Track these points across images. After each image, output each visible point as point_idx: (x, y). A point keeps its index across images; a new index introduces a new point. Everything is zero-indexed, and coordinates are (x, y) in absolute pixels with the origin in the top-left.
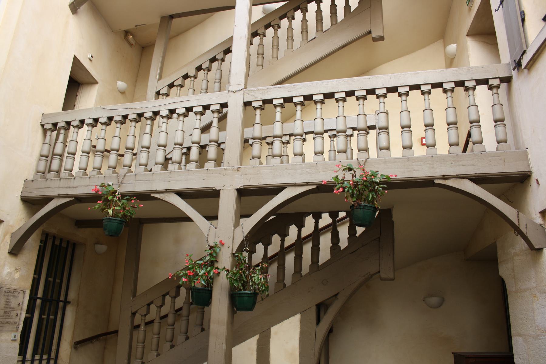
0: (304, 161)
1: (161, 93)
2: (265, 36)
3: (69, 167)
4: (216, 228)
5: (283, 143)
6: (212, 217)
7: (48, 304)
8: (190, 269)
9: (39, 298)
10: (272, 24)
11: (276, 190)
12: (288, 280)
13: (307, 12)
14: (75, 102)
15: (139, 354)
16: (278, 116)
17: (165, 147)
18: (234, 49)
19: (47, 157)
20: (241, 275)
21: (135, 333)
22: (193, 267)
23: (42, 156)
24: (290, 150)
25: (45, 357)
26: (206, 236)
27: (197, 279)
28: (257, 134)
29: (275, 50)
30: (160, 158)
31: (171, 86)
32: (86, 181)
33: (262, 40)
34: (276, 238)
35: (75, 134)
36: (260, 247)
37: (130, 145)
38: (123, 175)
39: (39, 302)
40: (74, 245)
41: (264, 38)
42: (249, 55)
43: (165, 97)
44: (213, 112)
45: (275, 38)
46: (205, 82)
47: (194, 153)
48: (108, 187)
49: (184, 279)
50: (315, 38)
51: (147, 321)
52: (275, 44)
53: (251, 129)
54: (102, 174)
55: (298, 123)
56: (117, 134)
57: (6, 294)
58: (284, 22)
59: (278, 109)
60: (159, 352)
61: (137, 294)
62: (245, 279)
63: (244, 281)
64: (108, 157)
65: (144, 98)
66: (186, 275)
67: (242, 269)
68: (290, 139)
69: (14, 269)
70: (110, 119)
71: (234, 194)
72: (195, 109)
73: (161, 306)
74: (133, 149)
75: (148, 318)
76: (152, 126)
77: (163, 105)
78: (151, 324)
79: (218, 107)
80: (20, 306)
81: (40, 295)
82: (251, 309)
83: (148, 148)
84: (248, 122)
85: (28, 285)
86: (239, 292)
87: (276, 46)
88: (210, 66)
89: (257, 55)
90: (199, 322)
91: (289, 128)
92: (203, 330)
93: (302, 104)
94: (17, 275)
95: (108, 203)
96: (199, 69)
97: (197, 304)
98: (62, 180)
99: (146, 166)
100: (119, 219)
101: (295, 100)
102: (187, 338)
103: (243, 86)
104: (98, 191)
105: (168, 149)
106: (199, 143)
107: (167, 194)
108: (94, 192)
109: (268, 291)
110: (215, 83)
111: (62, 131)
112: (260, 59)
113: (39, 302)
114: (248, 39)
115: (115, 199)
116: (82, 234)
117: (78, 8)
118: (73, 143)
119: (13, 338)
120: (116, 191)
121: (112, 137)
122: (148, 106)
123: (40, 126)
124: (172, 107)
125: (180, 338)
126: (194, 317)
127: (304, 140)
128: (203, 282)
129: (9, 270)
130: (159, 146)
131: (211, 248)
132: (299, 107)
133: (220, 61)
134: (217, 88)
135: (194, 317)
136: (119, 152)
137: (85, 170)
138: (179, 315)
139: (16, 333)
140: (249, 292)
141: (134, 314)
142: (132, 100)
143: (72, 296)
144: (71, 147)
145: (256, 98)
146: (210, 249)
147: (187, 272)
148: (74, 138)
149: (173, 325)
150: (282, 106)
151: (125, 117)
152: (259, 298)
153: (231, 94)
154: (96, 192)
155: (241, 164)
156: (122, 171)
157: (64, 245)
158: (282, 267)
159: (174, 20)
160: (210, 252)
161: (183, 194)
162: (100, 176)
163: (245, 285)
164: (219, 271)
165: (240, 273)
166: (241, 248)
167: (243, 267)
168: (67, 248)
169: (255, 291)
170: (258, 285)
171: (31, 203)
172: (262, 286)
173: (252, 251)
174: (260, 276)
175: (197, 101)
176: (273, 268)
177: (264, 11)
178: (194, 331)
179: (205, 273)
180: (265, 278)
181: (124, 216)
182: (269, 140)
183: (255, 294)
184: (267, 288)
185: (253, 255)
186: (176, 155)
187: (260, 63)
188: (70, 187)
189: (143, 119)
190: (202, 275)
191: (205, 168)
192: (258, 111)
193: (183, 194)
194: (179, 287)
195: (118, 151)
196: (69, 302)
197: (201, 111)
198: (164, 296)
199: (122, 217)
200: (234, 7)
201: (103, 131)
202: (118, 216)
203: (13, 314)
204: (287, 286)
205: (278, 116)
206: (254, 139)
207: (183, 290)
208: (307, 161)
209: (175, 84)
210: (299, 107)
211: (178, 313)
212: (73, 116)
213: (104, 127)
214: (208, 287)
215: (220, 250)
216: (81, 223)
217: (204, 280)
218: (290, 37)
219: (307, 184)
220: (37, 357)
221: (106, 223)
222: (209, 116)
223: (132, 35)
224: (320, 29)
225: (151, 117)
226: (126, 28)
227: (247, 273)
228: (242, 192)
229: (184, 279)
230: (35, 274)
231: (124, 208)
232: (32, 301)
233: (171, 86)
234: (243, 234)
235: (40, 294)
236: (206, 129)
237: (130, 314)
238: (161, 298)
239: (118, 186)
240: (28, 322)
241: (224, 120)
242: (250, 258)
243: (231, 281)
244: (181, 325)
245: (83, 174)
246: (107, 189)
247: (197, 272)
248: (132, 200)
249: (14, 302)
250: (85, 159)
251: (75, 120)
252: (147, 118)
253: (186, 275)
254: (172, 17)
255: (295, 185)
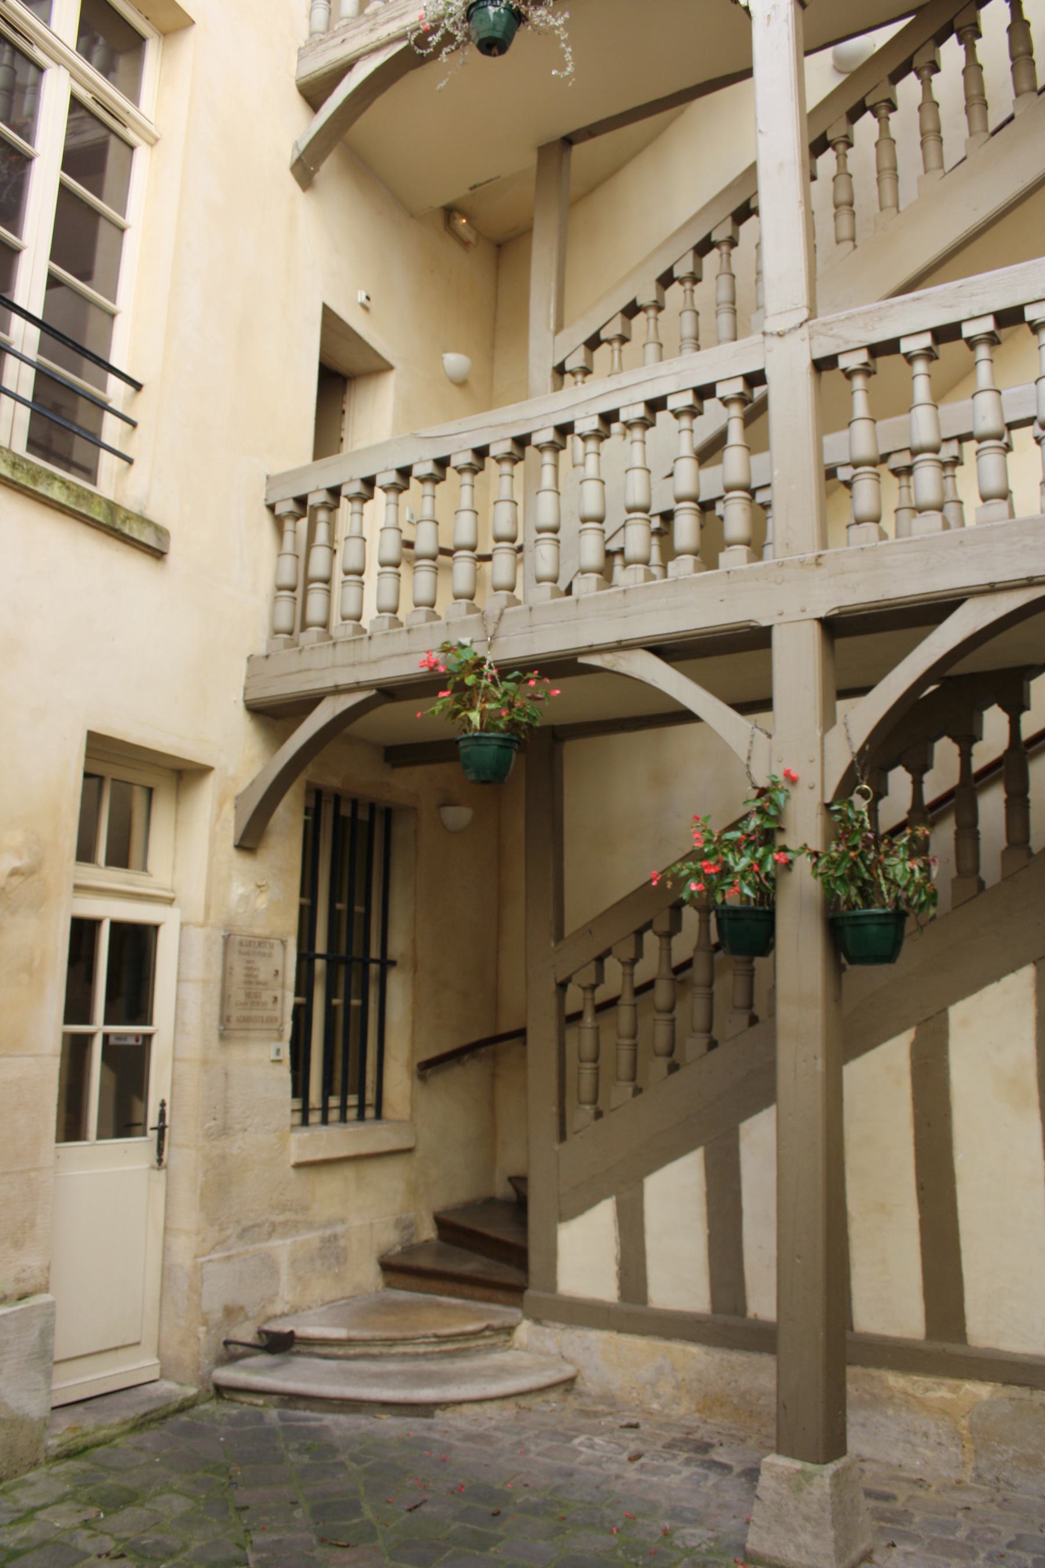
0: (1012, 514)
1: (568, 367)
2: (850, 145)
3: (351, 609)
4: (770, 736)
5: (944, 465)
6: (755, 703)
7: (342, 969)
8: (706, 857)
9: (320, 956)
10: (869, 102)
11: (936, 610)
12: (990, 868)
13: (979, 35)
14: (341, 429)
15: (586, 1091)
16: (921, 388)
17: (600, 520)
18: (765, 202)
19: (293, 589)
20: (855, 864)
21: (571, 1034)
22: (715, 852)
23: (280, 588)
24: (967, 484)
25: (352, 1100)
26: (744, 760)
27: (731, 884)
28: (864, 449)
29: (887, 183)
30: (591, 553)
31: (594, 343)
32: (400, 642)
33: (842, 159)
34: (945, 750)
35: (357, 517)
36: (899, 779)
37: (505, 529)
38: (497, 612)
39: (320, 965)
40: (388, 814)
41: (849, 152)
42: (809, 215)
43: (579, 377)
44: (726, 402)
45: (885, 144)
46: (688, 316)
47: (686, 528)
48: (460, 651)
49: (693, 886)
50: (1011, 118)
51: (598, 1001)
52: (886, 164)
53: (844, 434)
54: (439, 618)
55: (986, 400)
56: (466, 502)
57: (244, 949)
58: (909, 88)
59: (920, 366)
60: (639, 1082)
61: (568, 930)
62: (866, 876)
63: (864, 881)
64: (450, 569)
65: (522, 392)
66: (698, 874)
67: (855, 848)
68: (960, 450)
69: (252, 887)
70: (442, 463)
71: (813, 634)
72: (673, 403)
73: (634, 961)
74: (513, 540)
75: (602, 994)
76: (556, 466)
77: (581, 403)
78: (613, 1009)
79: (738, 386)
80: (280, 978)
81: (321, 947)
82: (889, 957)
83: (555, 530)
84: (831, 417)
85: (289, 924)
86: (852, 913)
87: (888, 171)
88: (698, 265)
89: (833, 210)
90: (740, 1000)
91: (891, 435)
92: (753, 1020)
93: (992, 339)
94: (261, 902)
95: (465, 695)
96: (666, 280)
97: (735, 950)
98: (339, 647)
99: (555, 580)
100: (502, 735)
101: (968, 330)
102: (713, 1045)
103: (805, 314)
104: (436, 664)
105: (610, 526)
106: (694, 499)
107: (621, 654)
108: (426, 669)
109: (935, 905)
110: (717, 314)
111: (322, 516)
112: (845, 219)
113: (320, 965)
114: (803, 165)
115: (484, 682)
116: (406, 784)
117: (314, 172)
118: (356, 543)
119: (273, 1057)
120: (484, 659)
121: (451, 512)
122: (539, 411)
123: (265, 512)
124: (606, 406)
125: (693, 1046)
126: (727, 984)
127: (1008, 448)
128: (747, 891)
129: (241, 891)
130: (584, 520)
131: (762, 792)
132: (983, 351)
133: (724, 248)
134: (725, 331)
135: (727, 984)
136: (480, 551)
137: (395, 611)
138: (682, 982)
139: (278, 1045)
140: (881, 911)
141: (563, 986)
142: (489, 401)
143: (398, 946)
144: (348, 555)
145: (847, 342)
146: (759, 796)
147: (699, 865)
148: (355, 531)
149: (671, 1010)
150: (929, 355)
151: (481, 453)
152: (910, 925)
153: (773, 342)
154: (431, 669)
155: (824, 545)
156: (491, 602)
157: (363, 815)
158: (968, 832)
159: (576, 149)
160: (758, 803)
161: (666, 650)
162: (435, 623)
163: (867, 891)
164: (789, 856)
165: (851, 859)
166: (847, 786)
167: (857, 840)
168: (371, 825)
169: (897, 907)
170: (906, 889)
171: (273, 715)
172: (918, 891)
173: (880, 792)
174: (908, 865)
175: (675, 377)
176: (943, 837)
177: (839, 66)
178: (730, 1023)
179: (750, 866)
180: (926, 869)
181: (513, 725)
182: (901, 460)
183: (899, 917)
184: (933, 898)
185: (882, 804)
186: (637, 539)
187: (845, 232)
188: (361, 663)
189: (530, 450)
190: (745, 871)
191: (722, 569)
192: (859, 382)
193: (666, 650)
194: (677, 907)
195: (473, 549)
196: (394, 963)
197: (691, 406)
198: (639, 933)
199: (508, 730)
200: (747, 73)
201: (428, 500)
202: (496, 728)
203: (267, 996)
204: (988, 885)
205: (921, 388)
206: (856, 465)
207: (690, 916)
208: (1020, 513)
209: (603, 336)
210: (983, 351)
211: (680, 977)
212: (344, 470)
213: (428, 487)
214: (761, 904)
215: (788, 797)
216: (400, 755)
217: (749, 885)
218: (931, 133)
219: (358, 687)
220: (334, 1101)
221: (469, 749)
222: (715, 415)
223: (464, 215)
224: (1025, 86)
225: (552, 442)
226: (446, 199)
227: (871, 856)
228: (835, 628)
229: (693, 886)
230: (302, 894)
231: (511, 705)
232: (305, 964)
233: (594, 343)
234: (851, 746)
235: (321, 946)
236: (710, 452)
237: (553, 987)
238: (632, 939)
239: (484, 645)
240: (302, 1016)
241: (762, 417)
242: (873, 810)
243: (826, 884)
244: (692, 1008)
245: (390, 627)
246: (459, 657)
247: (726, 863)
248: (528, 680)
249: (264, 970)
250: (389, 581)
251: (351, 480)
252: (540, 448)
253: (698, 874)
254: (568, 141)
255: (992, 589)
